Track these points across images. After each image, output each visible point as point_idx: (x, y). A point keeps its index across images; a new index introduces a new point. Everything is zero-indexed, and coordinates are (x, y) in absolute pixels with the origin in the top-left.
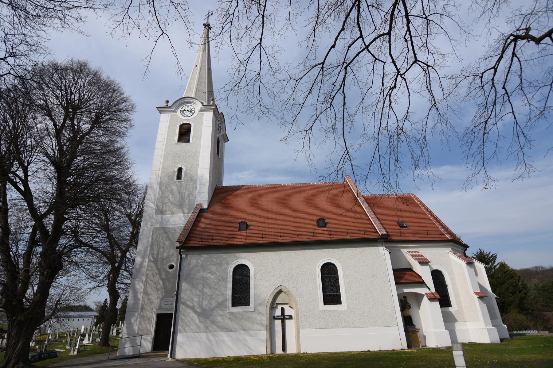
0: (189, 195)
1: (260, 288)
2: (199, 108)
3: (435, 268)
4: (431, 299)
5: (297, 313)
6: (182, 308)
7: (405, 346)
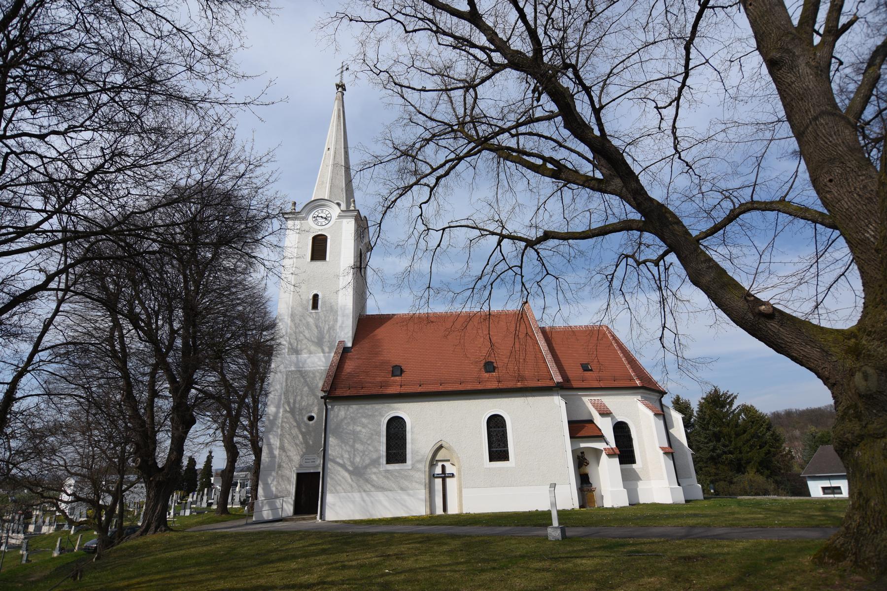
0: (329, 329)
1: (418, 443)
2: (337, 214)
3: (620, 419)
4: (610, 455)
5: (459, 471)
6: (330, 465)
7: (576, 506)
